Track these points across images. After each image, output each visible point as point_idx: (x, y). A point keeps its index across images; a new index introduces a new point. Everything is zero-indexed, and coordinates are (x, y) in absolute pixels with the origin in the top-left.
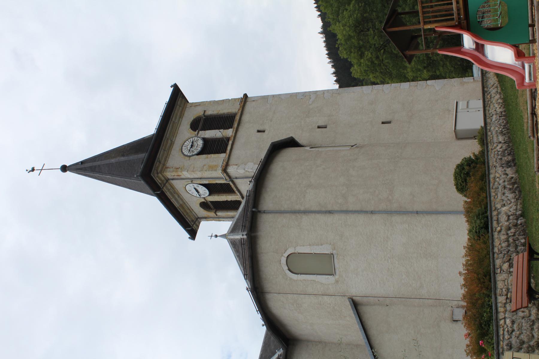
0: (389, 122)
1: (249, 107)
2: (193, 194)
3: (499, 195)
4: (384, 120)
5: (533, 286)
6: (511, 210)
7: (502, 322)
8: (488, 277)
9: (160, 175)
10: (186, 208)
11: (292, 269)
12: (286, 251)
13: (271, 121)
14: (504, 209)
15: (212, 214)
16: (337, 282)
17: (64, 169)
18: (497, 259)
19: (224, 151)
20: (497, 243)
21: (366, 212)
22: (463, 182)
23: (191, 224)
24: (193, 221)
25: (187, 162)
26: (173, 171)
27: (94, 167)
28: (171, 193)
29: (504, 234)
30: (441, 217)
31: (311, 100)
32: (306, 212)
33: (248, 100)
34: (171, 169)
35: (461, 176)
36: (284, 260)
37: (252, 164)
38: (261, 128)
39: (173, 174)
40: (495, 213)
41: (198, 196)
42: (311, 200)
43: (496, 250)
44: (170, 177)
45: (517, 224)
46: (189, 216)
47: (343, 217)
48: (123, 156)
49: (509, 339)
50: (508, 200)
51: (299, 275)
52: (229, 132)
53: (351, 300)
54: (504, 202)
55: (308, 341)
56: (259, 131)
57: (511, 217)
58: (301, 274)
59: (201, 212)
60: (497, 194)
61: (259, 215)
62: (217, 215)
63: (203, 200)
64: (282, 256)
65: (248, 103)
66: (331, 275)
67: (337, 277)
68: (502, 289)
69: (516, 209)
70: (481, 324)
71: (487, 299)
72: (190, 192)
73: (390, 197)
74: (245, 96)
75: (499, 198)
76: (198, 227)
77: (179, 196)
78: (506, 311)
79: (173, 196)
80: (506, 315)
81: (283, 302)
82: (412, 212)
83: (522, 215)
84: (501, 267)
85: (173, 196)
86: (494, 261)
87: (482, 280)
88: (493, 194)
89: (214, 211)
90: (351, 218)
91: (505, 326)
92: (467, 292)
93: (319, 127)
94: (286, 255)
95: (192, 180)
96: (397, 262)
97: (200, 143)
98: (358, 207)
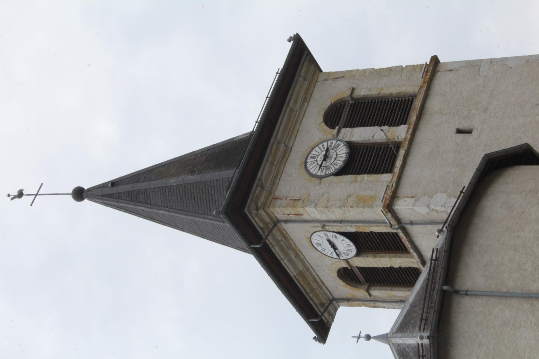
1: (441, 82)
2: (325, 253)
9: (261, 212)
10: (307, 274)
13: (485, 110)
15: (360, 293)
17: (79, 194)
19: (389, 170)
23: (319, 310)
24: (322, 304)
25: (316, 189)
27: (133, 193)
28: (282, 248)
33: (440, 68)
34: (284, 202)
37: (445, 195)
38: (464, 125)
41: (334, 255)
44: (280, 217)
46: (317, 296)
48: (192, 172)
52: (400, 132)
56: (459, 131)
59: (340, 288)
61: (456, 299)
63: (344, 265)
65: (438, 75)
72: (320, 249)
74: (435, 60)
76: (333, 316)
77: (297, 255)
79: (287, 255)
85: (287, 255)
89: (366, 287)
95: (324, 224)
97: (342, 152)
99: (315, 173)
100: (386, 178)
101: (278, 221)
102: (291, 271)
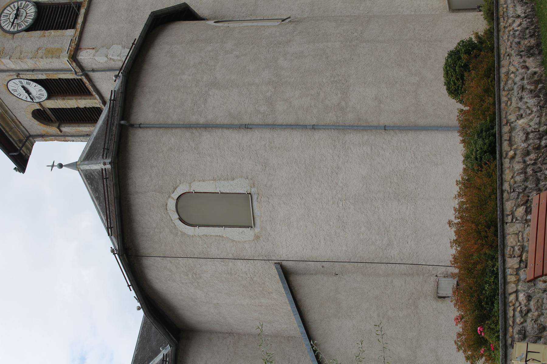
3: (514, 100)
6: (532, 124)
7: (512, 298)
8: (492, 229)
10: (6, 116)
11: (180, 200)
12: (175, 189)
14: (521, 122)
15: (53, 130)
16: (257, 237)
18: (507, 200)
19: (73, 27)
20: (508, 175)
21: (304, 127)
22: (458, 79)
23: (18, 145)
24: (20, 141)
29: (519, 162)
30: (423, 136)
32: (207, 127)
35: (455, 70)
36: (172, 204)
37: (120, 47)
40: (506, 129)
41: (29, 99)
42: (217, 107)
43: (506, 186)
45: (540, 145)
46: (15, 133)
47: (267, 134)
49: (522, 323)
50: (528, 107)
51: (197, 228)
53: (279, 266)
54: (522, 112)
57: (531, 136)
58: (200, 226)
59: (35, 126)
60: (510, 99)
61: (132, 131)
62: (61, 131)
63: (38, 107)
64: (169, 197)
66: (248, 227)
67: (257, 230)
68: (513, 247)
69: (540, 123)
70: (480, 302)
72: (16, 94)
73: (343, 103)
75: (514, 104)
76: (30, 151)
78: (519, 280)
80: (519, 287)
81: (171, 271)
82: (376, 128)
84: (512, 213)
86: (502, 204)
87: (483, 234)
88: (504, 99)
89: (57, 124)
91: (517, 304)
92: (460, 252)
94: (175, 195)
95: (18, 73)
96: (352, 207)
97: (31, 11)
98: (291, 119)
99: (8, 29)
100: (70, 33)
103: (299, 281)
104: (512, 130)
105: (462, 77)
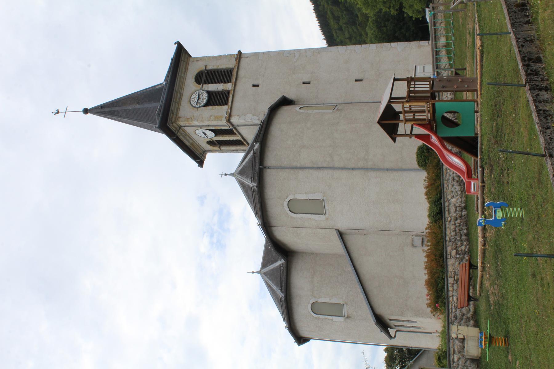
0: (361, 80)
1: (244, 62)
2: (201, 136)
3: (450, 186)
4: (357, 78)
5: (471, 294)
6: (458, 201)
7: (451, 299)
8: (442, 259)
9: (174, 124)
10: (195, 145)
12: (287, 197)
13: (263, 76)
14: (453, 200)
15: (217, 148)
16: (327, 219)
17: (86, 111)
19: (226, 103)
20: (448, 233)
21: (348, 169)
23: (200, 156)
24: (201, 154)
25: (196, 113)
26: (185, 121)
27: (111, 110)
28: (183, 136)
30: (405, 173)
31: (296, 58)
32: (302, 168)
33: (242, 56)
36: (286, 204)
38: (256, 83)
39: (185, 123)
40: (447, 204)
42: (305, 158)
43: (447, 238)
44: (182, 125)
45: (462, 215)
46: (198, 151)
47: (331, 172)
48: (138, 103)
50: (456, 191)
52: (229, 86)
54: (453, 194)
55: (303, 253)
56: (254, 86)
57: (458, 209)
59: (209, 147)
60: (448, 186)
61: (265, 170)
63: (210, 140)
65: (242, 59)
67: (327, 216)
69: (461, 202)
70: (437, 290)
71: (441, 274)
73: (366, 157)
74: (240, 52)
76: (205, 157)
77: (189, 137)
78: (453, 290)
79: (185, 138)
82: (383, 169)
83: (465, 208)
84: (450, 254)
86: (446, 248)
88: (445, 186)
90: (337, 173)
93: (304, 83)
95: (201, 127)
97: (205, 96)
98: (341, 165)
100: (226, 107)
101: (181, 126)
102: (187, 144)
103: (347, 238)
104: (449, 204)
105: (425, 161)
